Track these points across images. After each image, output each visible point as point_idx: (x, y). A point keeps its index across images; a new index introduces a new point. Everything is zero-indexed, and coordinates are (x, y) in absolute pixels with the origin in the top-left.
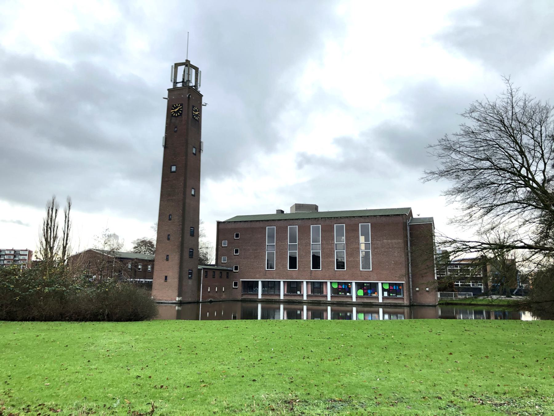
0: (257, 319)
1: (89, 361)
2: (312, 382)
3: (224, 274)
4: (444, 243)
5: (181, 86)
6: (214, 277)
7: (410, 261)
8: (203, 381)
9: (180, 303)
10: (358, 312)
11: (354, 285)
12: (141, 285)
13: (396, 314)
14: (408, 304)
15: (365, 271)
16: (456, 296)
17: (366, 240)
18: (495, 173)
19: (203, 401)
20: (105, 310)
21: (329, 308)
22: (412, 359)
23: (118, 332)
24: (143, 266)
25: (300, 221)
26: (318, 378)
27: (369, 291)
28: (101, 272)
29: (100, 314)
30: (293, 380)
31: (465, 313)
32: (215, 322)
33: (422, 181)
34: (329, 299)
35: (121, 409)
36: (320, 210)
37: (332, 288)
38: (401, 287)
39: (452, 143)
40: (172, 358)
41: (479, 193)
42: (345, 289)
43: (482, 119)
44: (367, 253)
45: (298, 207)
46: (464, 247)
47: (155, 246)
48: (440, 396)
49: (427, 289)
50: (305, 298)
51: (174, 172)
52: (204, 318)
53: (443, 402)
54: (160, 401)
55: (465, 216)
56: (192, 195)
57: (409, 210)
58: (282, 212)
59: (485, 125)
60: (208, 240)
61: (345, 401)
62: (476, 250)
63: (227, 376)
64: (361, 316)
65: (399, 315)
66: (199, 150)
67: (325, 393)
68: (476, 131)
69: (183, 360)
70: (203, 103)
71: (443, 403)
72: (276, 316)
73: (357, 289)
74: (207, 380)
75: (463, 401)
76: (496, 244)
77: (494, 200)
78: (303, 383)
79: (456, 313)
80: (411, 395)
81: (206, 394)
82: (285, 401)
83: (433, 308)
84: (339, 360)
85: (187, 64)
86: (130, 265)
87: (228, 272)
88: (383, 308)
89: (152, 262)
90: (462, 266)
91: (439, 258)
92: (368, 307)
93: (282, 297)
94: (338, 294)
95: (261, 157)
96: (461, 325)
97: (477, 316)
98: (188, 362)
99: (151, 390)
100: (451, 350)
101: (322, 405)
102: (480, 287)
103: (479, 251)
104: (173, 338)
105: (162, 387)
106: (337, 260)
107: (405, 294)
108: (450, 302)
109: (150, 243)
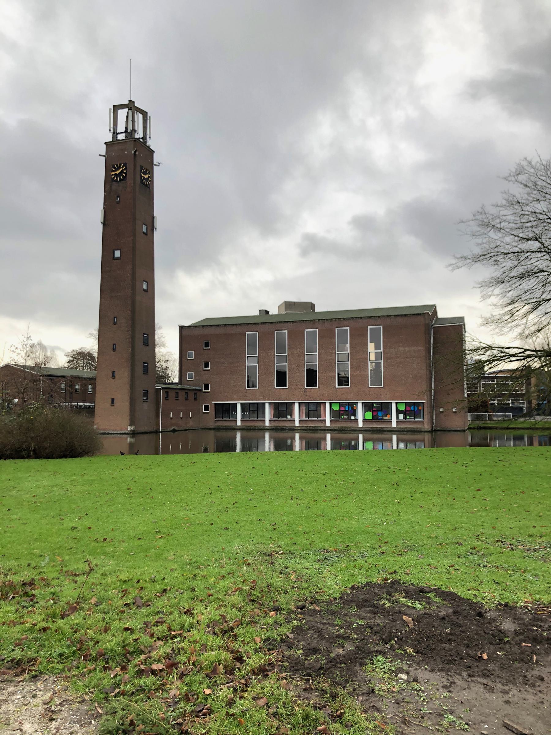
0: (234, 450)
1: (9, 510)
2: (300, 528)
3: (191, 395)
4: (476, 350)
5: (124, 138)
6: (177, 399)
7: (433, 373)
8: (159, 532)
9: (133, 434)
10: (365, 440)
11: (360, 405)
12: (79, 410)
13: (414, 441)
14: (430, 429)
15: (374, 387)
16: (490, 418)
17: (377, 347)
18: (545, 257)
19: (159, 556)
20: (30, 444)
21: (328, 436)
22: (430, 498)
23: (49, 472)
24: (81, 386)
25: (290, 325)
26: (308, 523)
27: (380, 414)
28: (23, 394)
29: (24, 450)
30: (277, 526)
31: (501, 439)
32: (177, 456)
33: (450, 268)
34: (328, 424)
35: (50, 569)
36: (317, 310)
37: (332, 410)
38: (420, 408)
39: (490, 217)
40: (120, 503)
41: (524, 285)
42: (350, 411)
43: (530, 184)
44: (378, 365)
45: (288, 305)
46: (503, 354)
47: (97, 360)
48: (460, 541)
49: (454, 410)
50: (297, 423)
51: (118, 259)
52: (166, 451)
53: (464, 549)
54: (102, 557)
55: (504, 314)
56: (144, 290)
57: (433, 308)
58: (267, 312)
59: (535, 192)
60: (168, 348)
61: (341, 552)
62: (518, 358)
63: (191, 524)
64: (369, 445)
65: (417, 444)
66: (152, 228)
67: (317, 542)
68: (523, 201)
69: (134, 505)
70: (155, 163)
71: (463, 550)
72: (260, 447)
73: (365, 410)
74: (165, 530)
75: (489, 546)
76: (544, 351)
77: (543, 292)
78: (288, 530)
79: (491, 439)
80: (425, 542)
81: (162, 548)
82: (265, 554)
83: (462, 433)
84: (337, 501)
85: (131, 106)
86: (63, 385)
87: (197, 392)
88: (397, 435)
89: (93, 380)
90: (499, 380)
91: (471, 369)
92: (378, 433)
93: (267, 423)
94: (340, 418)
95: (252, 241)
96: (495, 454)
97: (517, 442)
98: (141, 508)
99: (90, 544)
100: (480, 485)
101: (312, 557)
102: (521, 405)
103: (521, 360)
104: (121, 478)
105: (105, 540)
106: (338, 374)
107: (426, 417)
108: (484, 425)
109: (90, 354)
